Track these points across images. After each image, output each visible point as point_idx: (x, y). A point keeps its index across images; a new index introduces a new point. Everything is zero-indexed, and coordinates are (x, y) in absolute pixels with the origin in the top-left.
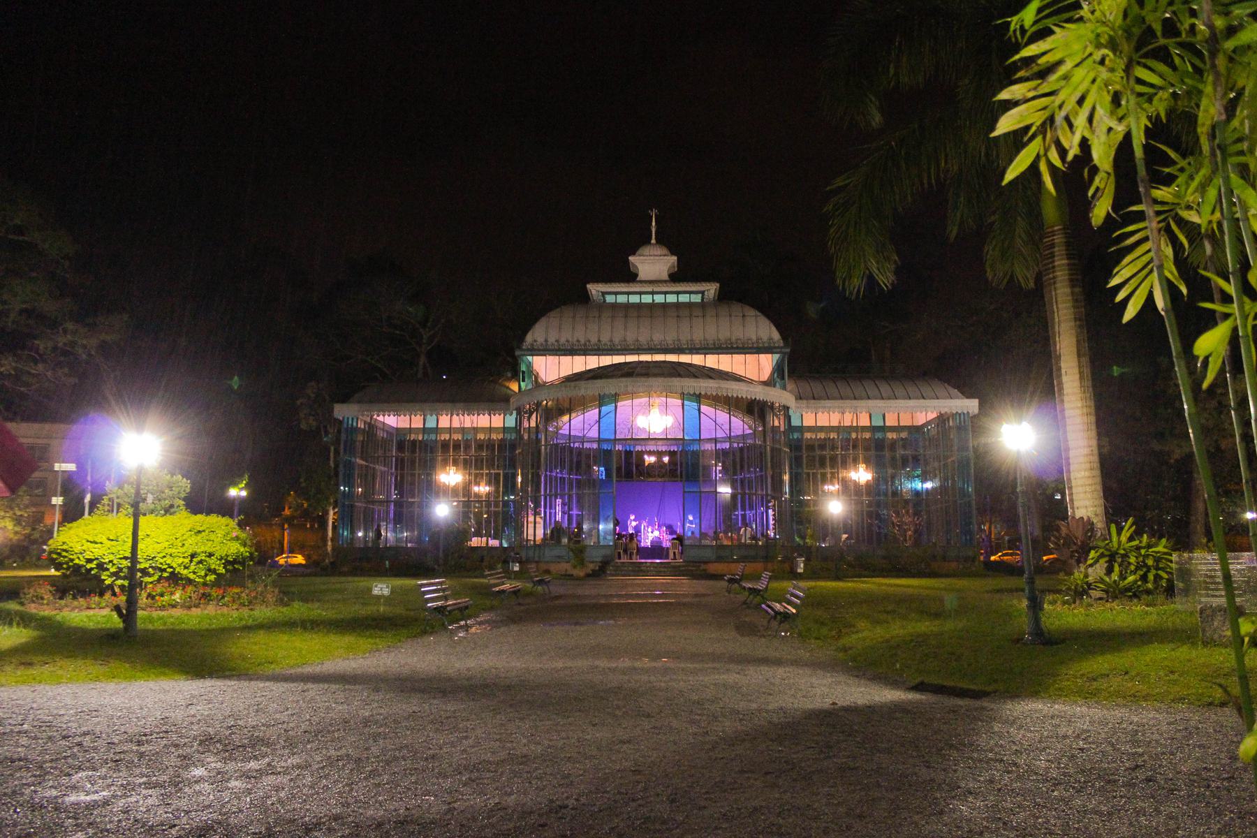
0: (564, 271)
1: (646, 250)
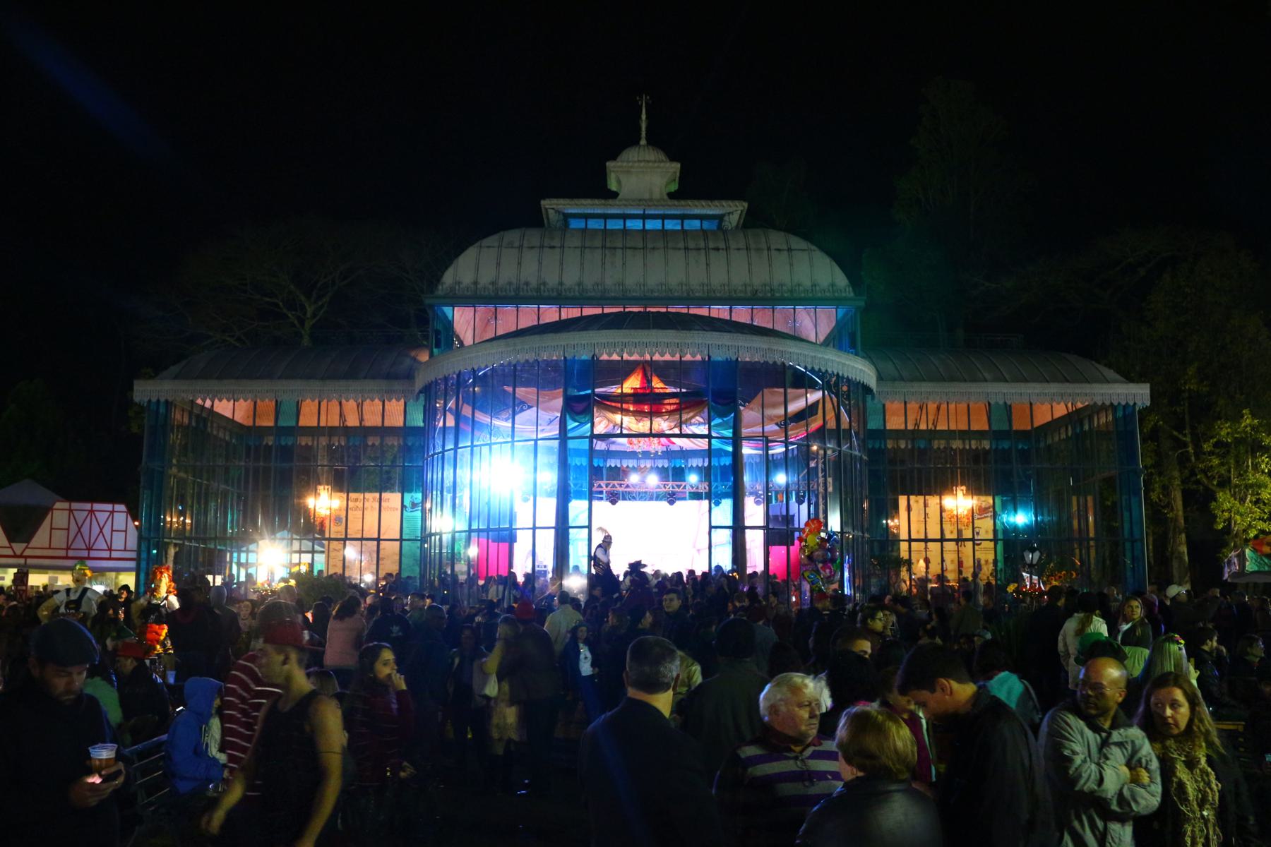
0: (120, 502)
1: (630, 155)
